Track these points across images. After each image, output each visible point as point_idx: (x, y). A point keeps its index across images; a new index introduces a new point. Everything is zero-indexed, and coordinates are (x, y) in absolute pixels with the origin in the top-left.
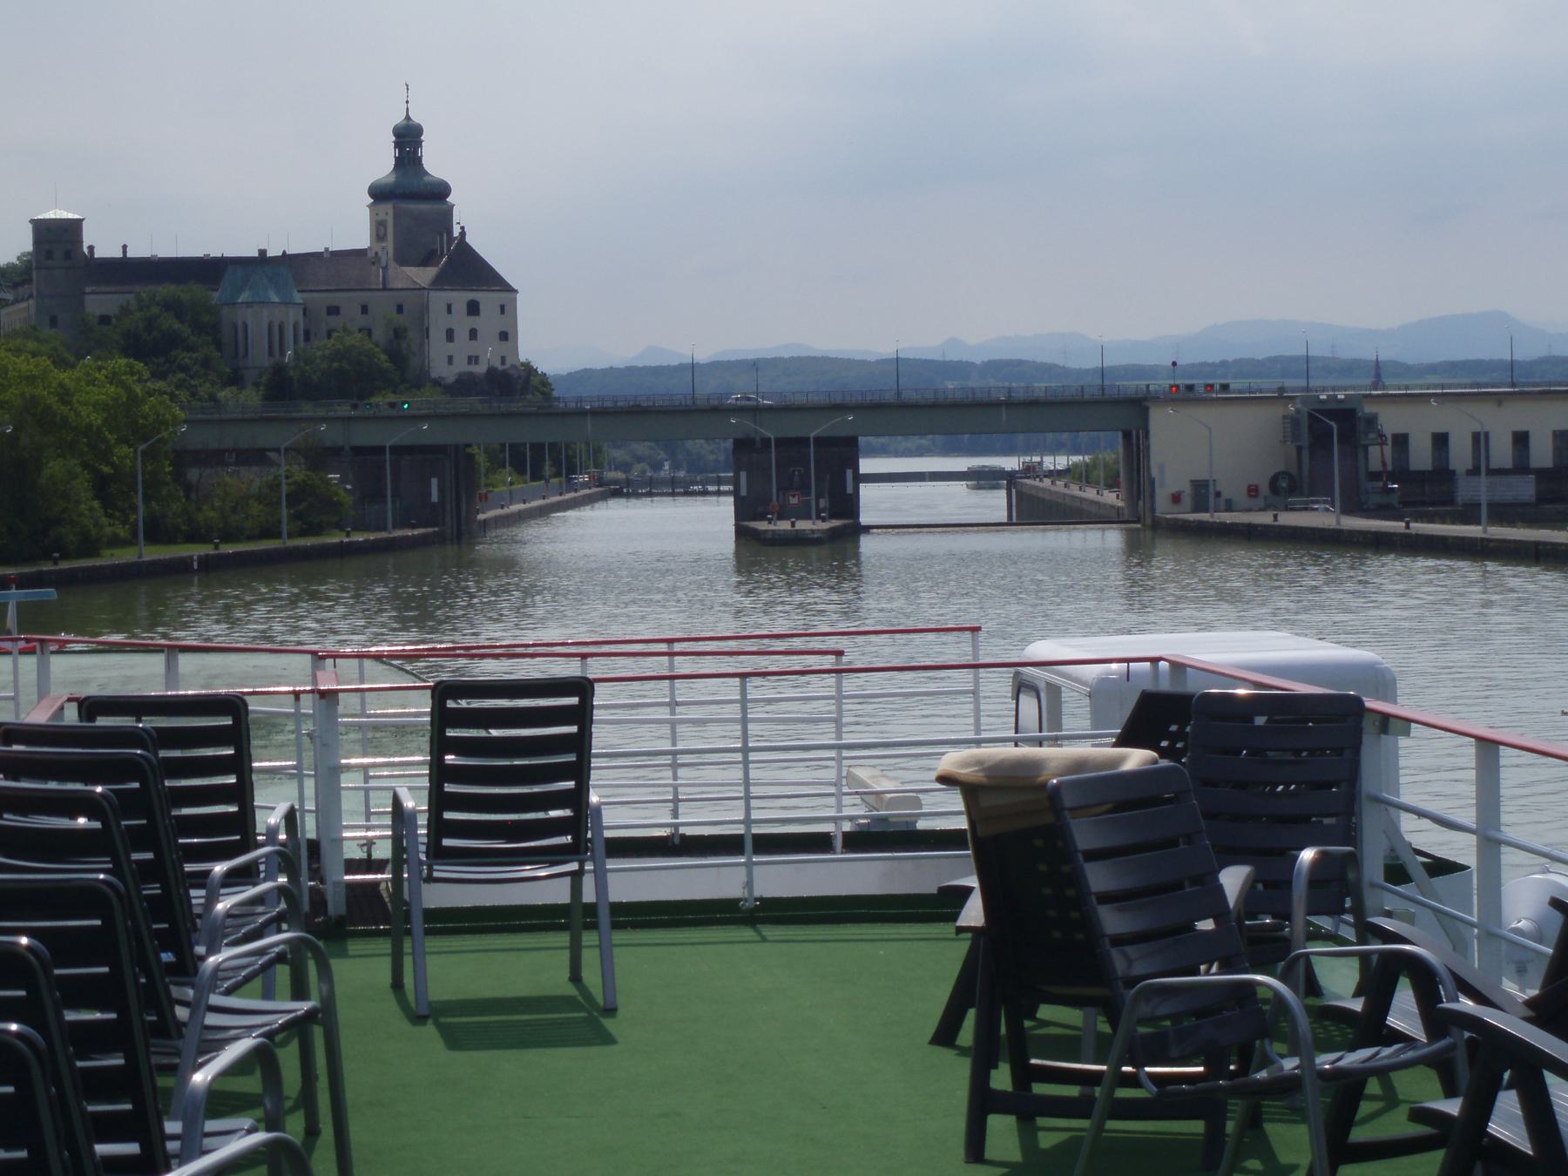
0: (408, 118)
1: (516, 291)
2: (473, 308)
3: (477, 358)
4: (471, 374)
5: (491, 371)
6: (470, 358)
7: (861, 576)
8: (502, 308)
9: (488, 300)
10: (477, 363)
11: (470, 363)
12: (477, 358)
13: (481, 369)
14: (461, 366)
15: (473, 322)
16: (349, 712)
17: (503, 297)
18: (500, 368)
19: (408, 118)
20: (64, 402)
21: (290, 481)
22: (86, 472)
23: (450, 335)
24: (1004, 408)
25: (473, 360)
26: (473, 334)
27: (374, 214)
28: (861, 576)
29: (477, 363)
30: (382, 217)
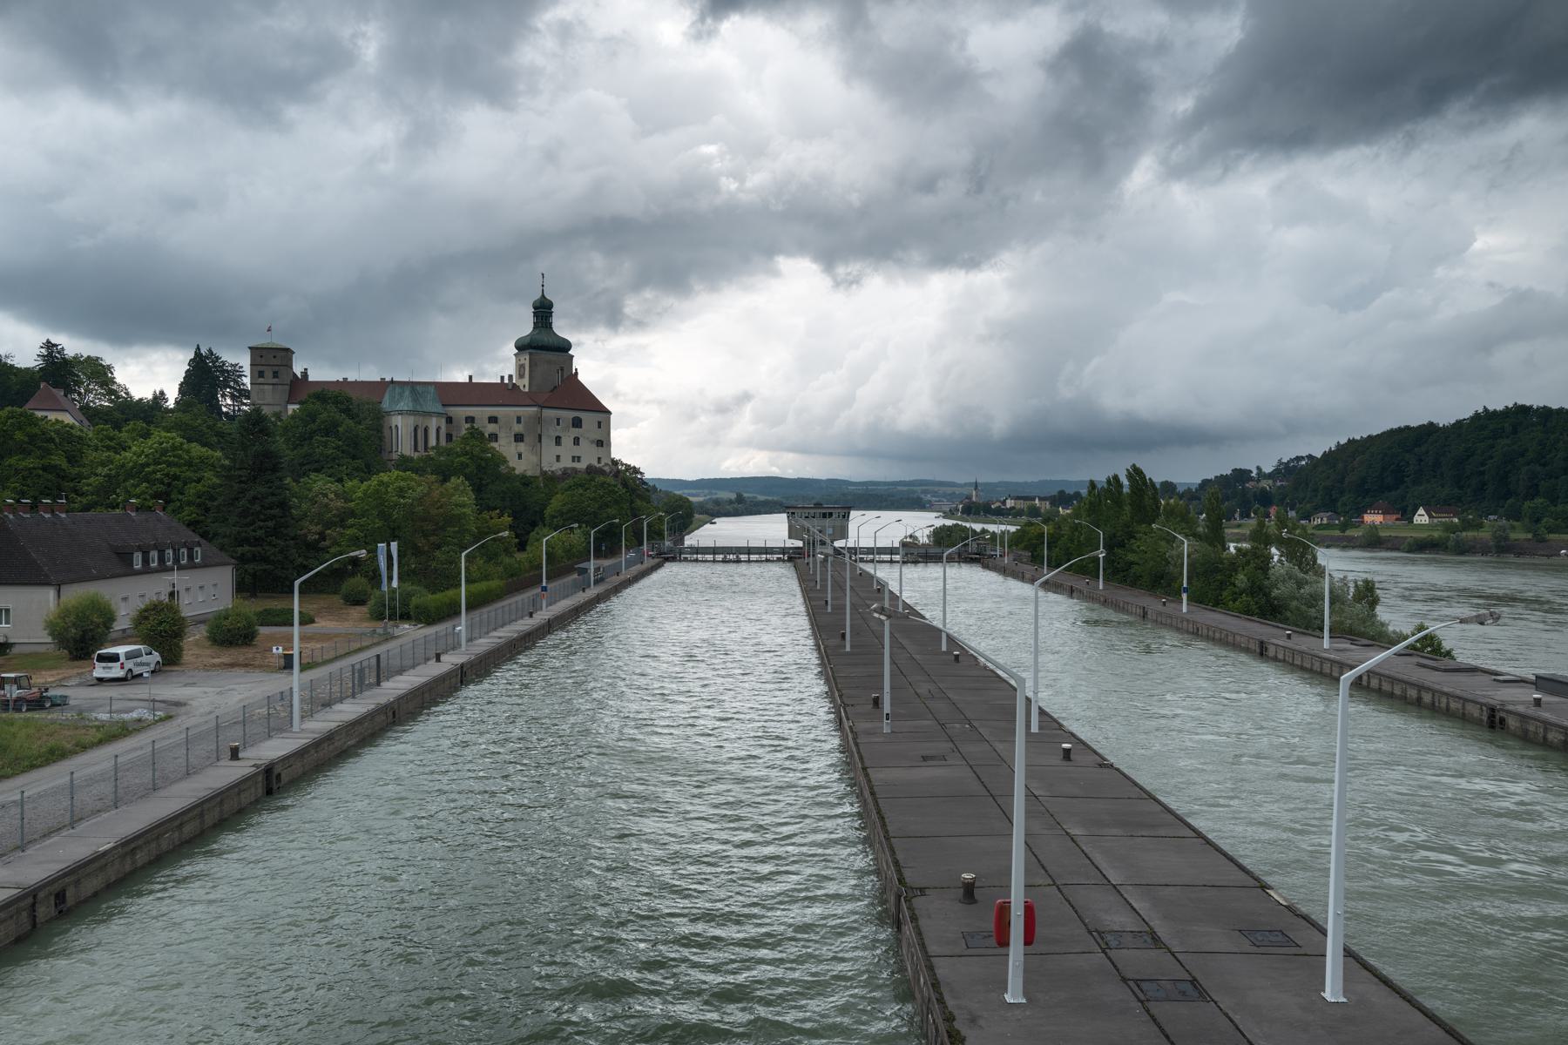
0: (543, 295)
1: (609, 413)
2: (577, 423)
3: (579, 458)
4: (575, 470)
5: (590, 469)
6: (573, 457)
7: (1346, 919)
8: (599, 423)
9: (586, 417)
10: (579, 461)
11: (573, 461)
12: (579, 458)
13: (582, 465)
14: (567, 463)
15: (575, 432)
16: (948, 616)
17: (600, 416)
18: (598, 466)
19: (543, 295)
20: (347, 500)
21: (310, 628)
22: (728, 157)
23: (558, 441)
24: (858, 741)
25: (576, 459)
26: (576, 441)
27: (518, 360)
28: (1346, 919)
29: (579, 461)
30: (522, 362)
